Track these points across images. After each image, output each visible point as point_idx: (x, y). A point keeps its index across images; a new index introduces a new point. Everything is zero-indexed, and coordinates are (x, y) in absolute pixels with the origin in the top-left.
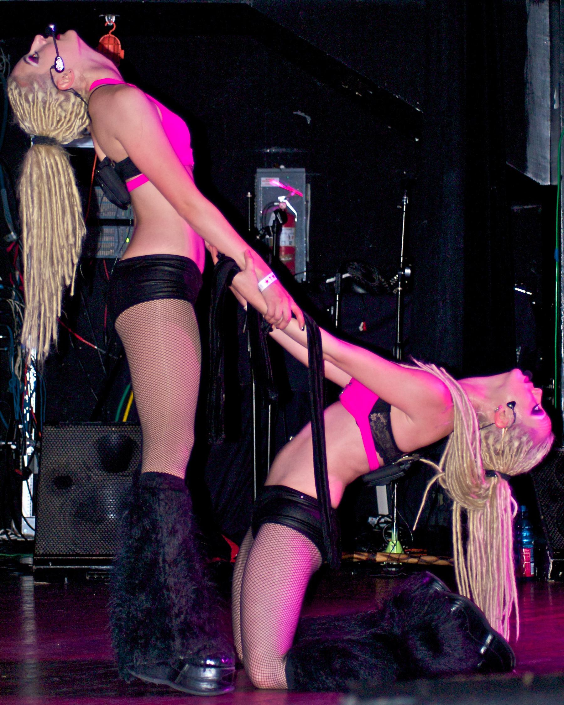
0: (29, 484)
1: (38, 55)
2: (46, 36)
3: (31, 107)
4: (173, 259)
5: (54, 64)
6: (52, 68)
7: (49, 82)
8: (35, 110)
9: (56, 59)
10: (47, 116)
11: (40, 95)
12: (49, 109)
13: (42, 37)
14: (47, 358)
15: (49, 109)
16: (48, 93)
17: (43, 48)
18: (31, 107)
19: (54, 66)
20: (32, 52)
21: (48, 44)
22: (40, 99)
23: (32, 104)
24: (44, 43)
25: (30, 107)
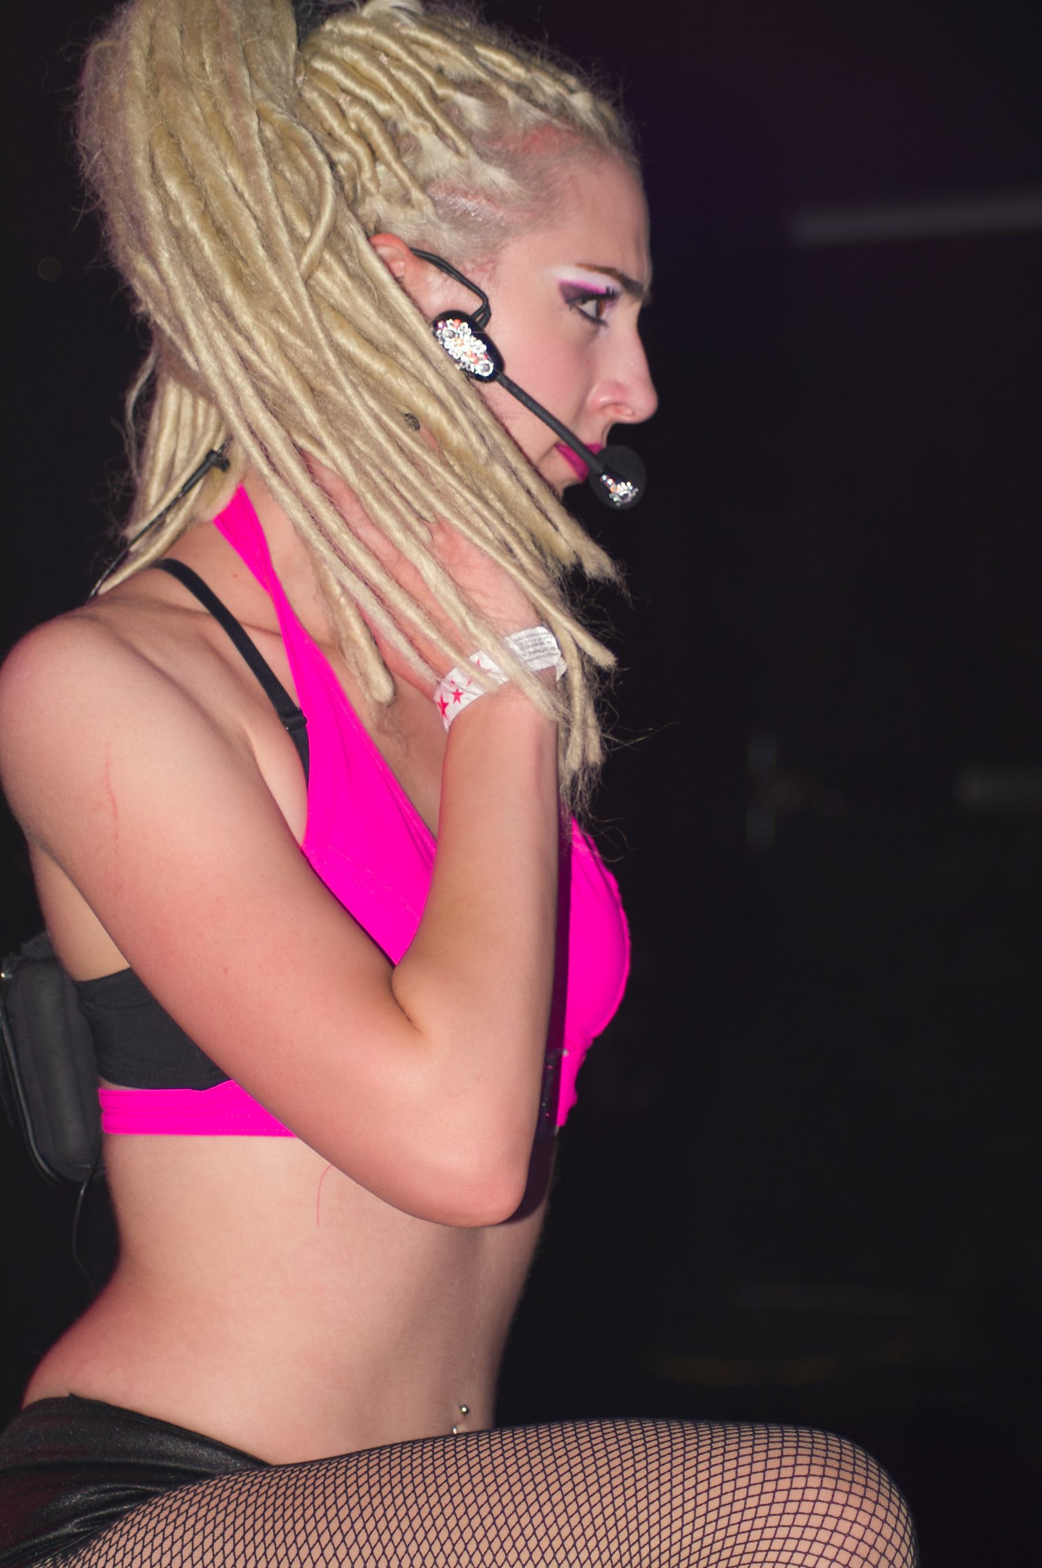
0: (247, 213)
1: (585, 315)
2: (619, 432)
3: (430, 78)
4: (409, 808)
5: (491, 330)
6: (486, 311)
7: (447, 241)
8: (407, 80)
9: (493, 352)
10: (343, 100)
11: (439, 157)
12: (362, 135)
13: (626, 417)
14: (637, 817)
15: (362, 135)
16: (416, 194)
17: (584, 355)
18: (430, 78)
19: (478, 324)
20: (623, 318)
21: (580, 410)
22: (427, 138)
23: (441, 91)
24: (599, 396)
25: (439, 72)
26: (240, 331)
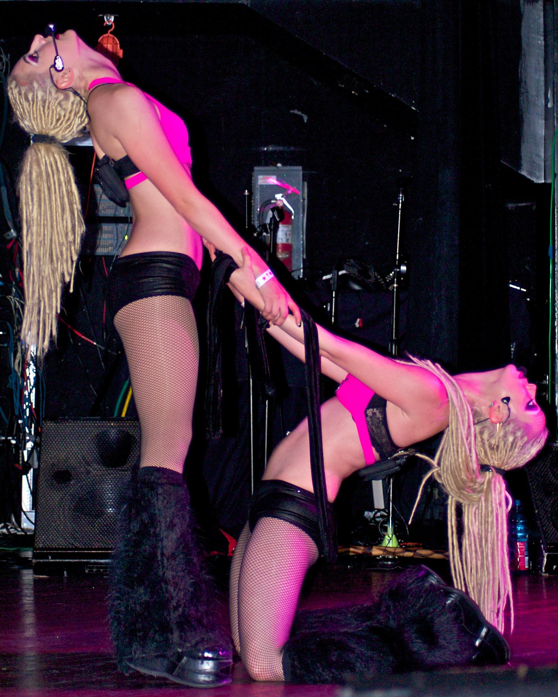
0: (29, 479)
1: (37, 54)
2: (45, 36)
3: (31, 106)
5: (53, 63)
6: (51, 67)
7: (48, 81)
8: (35, 109)
9: (56, 59)
10: (46, 115)
11: (40, 94)
12: (49, 108)
13: (42, 37)
14: (47, 354)
15: (49, 108)
16: (48, 92)
17: (43, 48)
18: (31, 106)
19: (54, 66)
20: (32, 51)
21: (48, 43)
22: (40, 98)
23: (32, 103)
24: (44, 42)
25: (29, 105)
26: (42, 290)
